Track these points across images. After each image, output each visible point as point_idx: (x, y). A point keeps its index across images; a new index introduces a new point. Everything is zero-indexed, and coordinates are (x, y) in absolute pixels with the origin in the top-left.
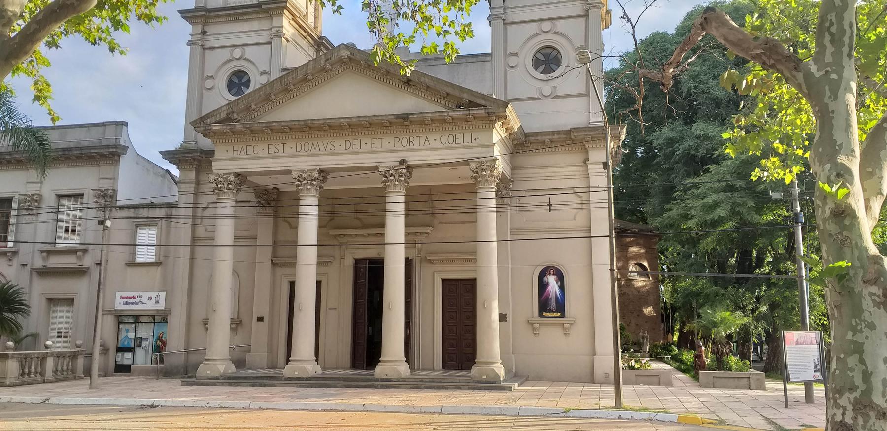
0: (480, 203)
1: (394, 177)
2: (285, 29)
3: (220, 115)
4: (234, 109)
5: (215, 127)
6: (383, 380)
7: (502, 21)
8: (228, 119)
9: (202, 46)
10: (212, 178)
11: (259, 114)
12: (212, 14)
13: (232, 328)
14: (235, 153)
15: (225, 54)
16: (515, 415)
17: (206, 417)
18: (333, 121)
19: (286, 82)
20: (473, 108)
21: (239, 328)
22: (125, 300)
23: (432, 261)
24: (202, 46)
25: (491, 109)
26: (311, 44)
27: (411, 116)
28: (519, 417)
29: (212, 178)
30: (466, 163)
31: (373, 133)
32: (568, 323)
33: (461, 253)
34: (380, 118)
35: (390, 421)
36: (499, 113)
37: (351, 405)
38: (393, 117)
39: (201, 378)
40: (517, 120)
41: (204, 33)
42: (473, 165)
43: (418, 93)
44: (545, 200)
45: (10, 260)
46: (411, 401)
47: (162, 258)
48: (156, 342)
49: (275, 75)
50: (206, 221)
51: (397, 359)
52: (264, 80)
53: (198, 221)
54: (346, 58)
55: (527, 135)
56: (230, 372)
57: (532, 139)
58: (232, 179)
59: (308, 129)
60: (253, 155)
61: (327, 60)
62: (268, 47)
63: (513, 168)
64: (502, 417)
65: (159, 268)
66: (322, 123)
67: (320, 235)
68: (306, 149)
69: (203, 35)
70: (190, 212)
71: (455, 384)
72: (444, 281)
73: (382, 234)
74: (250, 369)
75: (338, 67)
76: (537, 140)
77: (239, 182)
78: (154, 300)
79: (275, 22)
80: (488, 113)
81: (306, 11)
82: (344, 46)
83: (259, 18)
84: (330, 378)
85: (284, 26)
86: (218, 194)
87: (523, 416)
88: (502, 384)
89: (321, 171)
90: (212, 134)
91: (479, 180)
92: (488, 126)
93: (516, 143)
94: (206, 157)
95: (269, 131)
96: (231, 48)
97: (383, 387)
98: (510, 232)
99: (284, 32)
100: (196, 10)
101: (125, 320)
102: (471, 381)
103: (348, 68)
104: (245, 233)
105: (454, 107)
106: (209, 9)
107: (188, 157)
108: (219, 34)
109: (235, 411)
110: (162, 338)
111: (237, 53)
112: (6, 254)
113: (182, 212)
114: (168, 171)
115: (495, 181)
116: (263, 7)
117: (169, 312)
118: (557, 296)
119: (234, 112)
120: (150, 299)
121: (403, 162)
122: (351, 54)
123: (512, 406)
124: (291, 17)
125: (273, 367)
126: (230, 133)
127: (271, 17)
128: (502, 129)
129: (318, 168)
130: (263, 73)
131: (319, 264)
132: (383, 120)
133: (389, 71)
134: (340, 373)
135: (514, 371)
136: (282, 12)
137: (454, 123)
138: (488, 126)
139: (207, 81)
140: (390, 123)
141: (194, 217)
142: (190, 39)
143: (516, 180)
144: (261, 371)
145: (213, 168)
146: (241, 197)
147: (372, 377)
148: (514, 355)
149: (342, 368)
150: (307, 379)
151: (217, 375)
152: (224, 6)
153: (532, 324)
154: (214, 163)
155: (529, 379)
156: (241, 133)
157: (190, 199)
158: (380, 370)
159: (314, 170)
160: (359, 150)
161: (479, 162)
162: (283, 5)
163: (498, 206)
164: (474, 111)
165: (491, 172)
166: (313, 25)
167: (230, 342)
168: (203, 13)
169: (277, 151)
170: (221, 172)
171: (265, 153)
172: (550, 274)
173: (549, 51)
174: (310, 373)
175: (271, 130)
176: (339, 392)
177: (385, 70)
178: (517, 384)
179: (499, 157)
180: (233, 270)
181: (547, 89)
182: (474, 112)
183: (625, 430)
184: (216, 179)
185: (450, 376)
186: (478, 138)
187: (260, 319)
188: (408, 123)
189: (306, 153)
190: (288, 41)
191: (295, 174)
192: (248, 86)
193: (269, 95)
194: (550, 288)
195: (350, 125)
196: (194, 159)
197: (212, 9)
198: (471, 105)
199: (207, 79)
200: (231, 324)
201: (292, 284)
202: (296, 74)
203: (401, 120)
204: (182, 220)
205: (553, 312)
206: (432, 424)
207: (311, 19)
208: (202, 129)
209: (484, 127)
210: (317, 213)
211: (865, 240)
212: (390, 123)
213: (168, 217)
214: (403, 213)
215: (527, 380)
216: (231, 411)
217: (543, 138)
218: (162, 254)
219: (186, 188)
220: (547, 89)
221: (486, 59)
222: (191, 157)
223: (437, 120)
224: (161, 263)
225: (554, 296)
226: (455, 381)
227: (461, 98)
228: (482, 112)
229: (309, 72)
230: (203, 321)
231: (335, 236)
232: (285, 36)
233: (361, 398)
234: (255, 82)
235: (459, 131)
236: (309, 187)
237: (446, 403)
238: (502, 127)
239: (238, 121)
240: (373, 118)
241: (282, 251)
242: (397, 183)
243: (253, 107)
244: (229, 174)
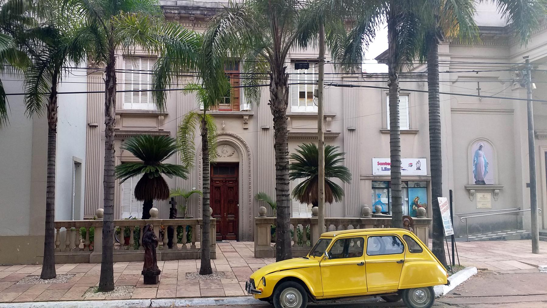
22: (384, 166)
45: (246, 123)
48: (412, 206)
65: (417, 136)
78: (415, 167)
101: (376, 185)
110: (417, 202)
112: (243, 117)
120: (411, 165)
211: (323, 94)
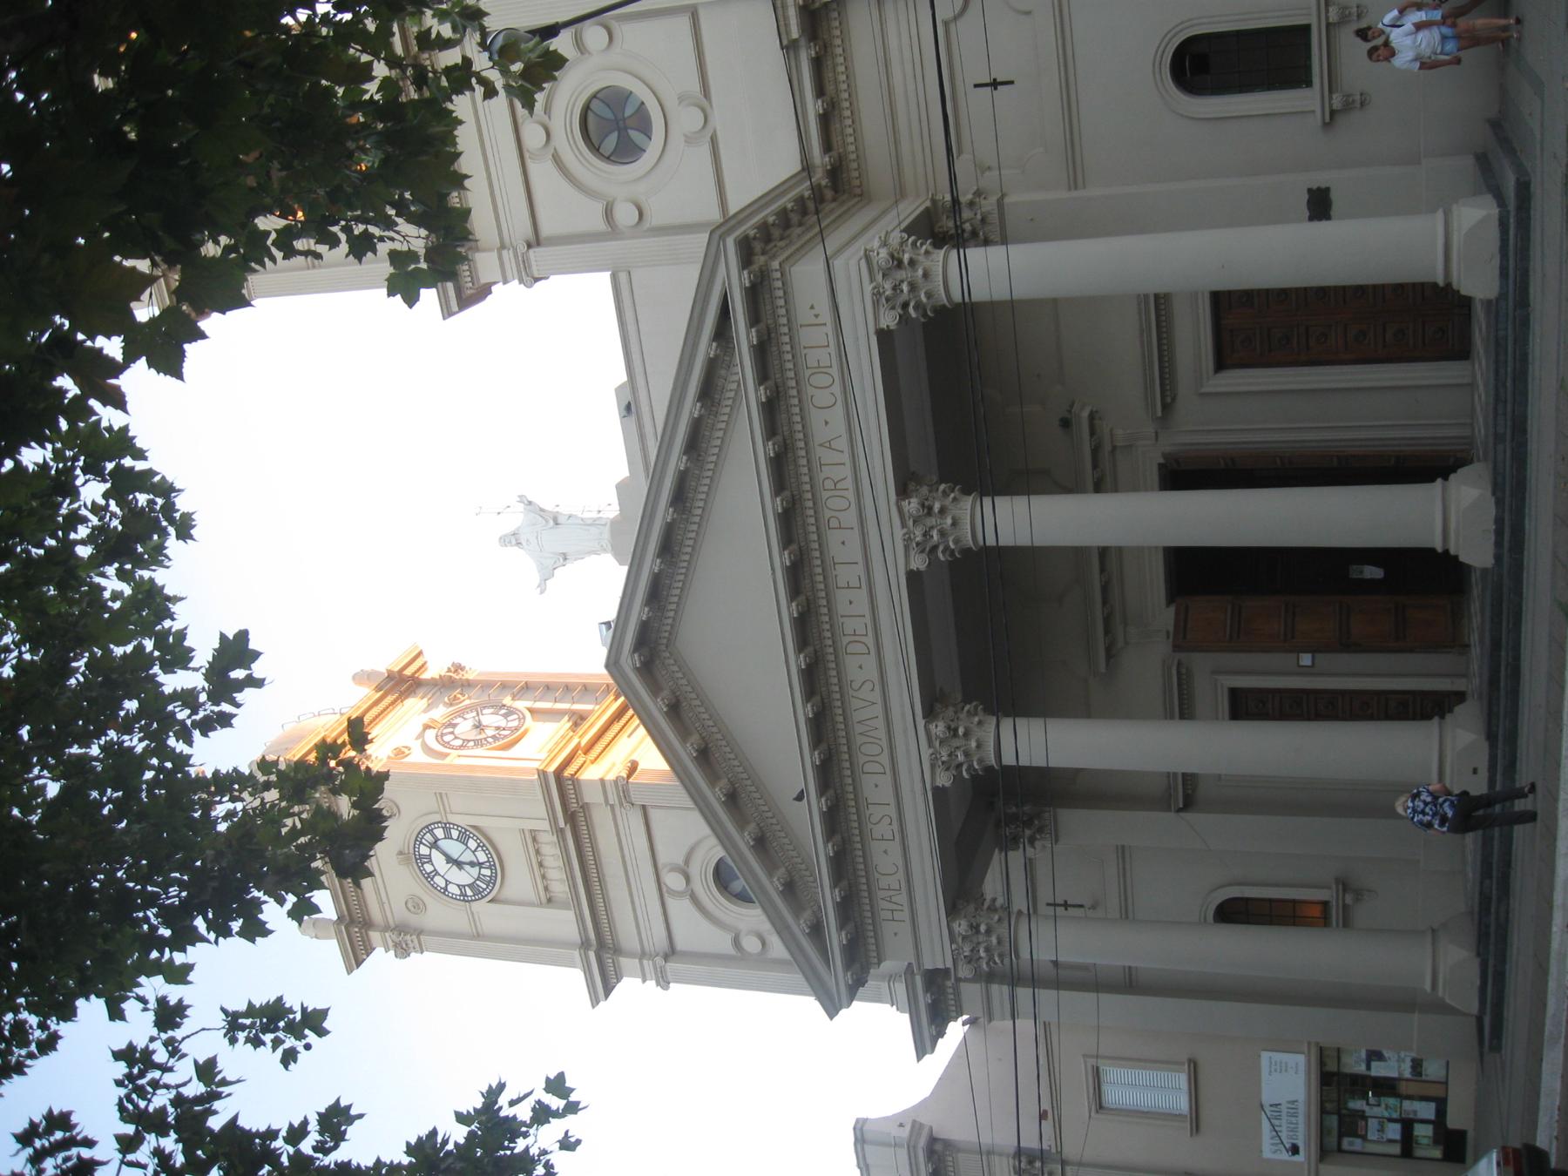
2: (608, 772)
7: (531, 251)
15: (681, 910)
32: (1327, 11)
58: (964, 923)
60: (901, 875)
68: (875, 750)
79: (592, 797)
85: (600, 776)
111: (674, 881)
127: (585, 807)
129: (921, 722)
153: (1333, 113)
158: (1476, 552)
160: (868, 620)
183: (1566, 757)
186: (812, 307)
199: (743, 949)
220: (687, 120)
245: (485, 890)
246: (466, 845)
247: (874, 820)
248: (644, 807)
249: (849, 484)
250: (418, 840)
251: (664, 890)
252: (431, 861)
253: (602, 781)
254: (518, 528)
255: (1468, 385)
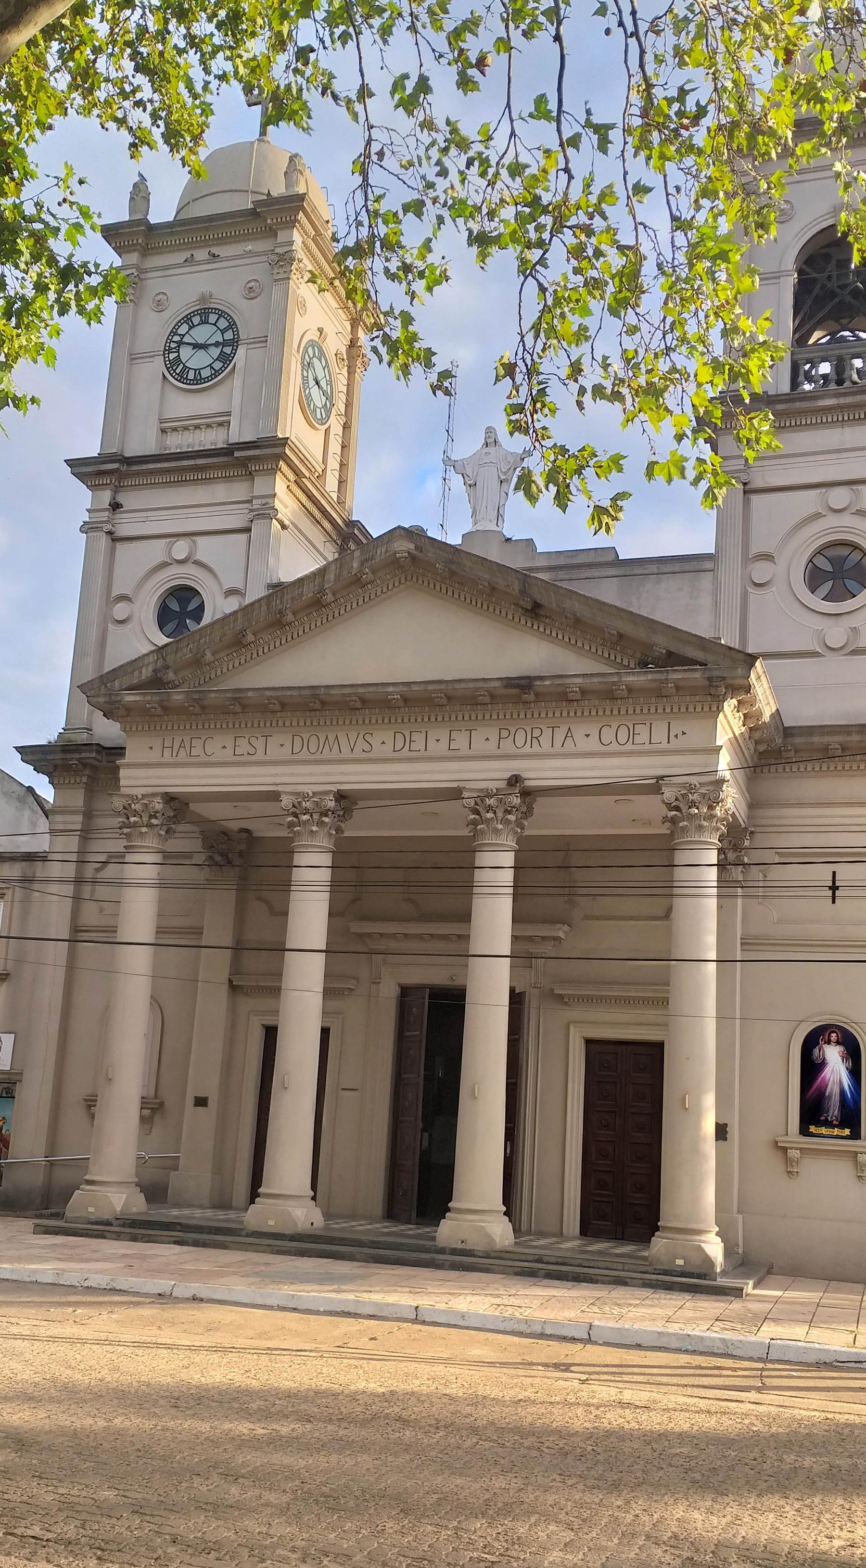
0: (681, 874)
1: (495, 813)
3: (141, 673)
4: (170, 660)
5: (130, 698)
6: (454, 1252)
8: (156, 682)
9: (110, 533)
10: (118, 803)
11: (219, 673)
12: (135, 468)
13: (142, 1119)
14: (167, 752)
15: (156, 551)
16: (760, 1360)
17: (79, 1311)
18: (371, 689)
19: (279, 607)
20: (675, 668)
21: (157, 1119)
23: (566, 1000)
24: (110, 533)
25: (716, 669)
26: (330, 536)
27: (538, 683)
28: (770, 1366)
29: (118, 803)
30: (655, 786)
31: (453, 718)
32: (796, 1149)
33: (629, 984)
34: (471, 685)
35: (476, 1352)
36: (733, 678)
37: (388, 1305)
38: (497, 684)
39: (76, 1220)
40: (770, 698)
41: (115, 506)
42: (669, 794)
43: (554, 634)
44: (822, 873)
46: (520, 1307)
47: (10, 966)
49: (256, 592)
50: (102, 892)
51: (486, 1209)
52: (232, 605)
53: (87, 890)
54: (406, 558)
55: (788, 732)
56: (134, 1210)
57: (798, 740)
59: (318, 706)
60: (203, 758)
61: (367, 560)
62: (243, 537)
63: (753, 805)
64: (728, 1363)
66: (349, 695)
67: (332, 931)
69: (114, 510)
70: (70, 871)
71: (615, 1273)
72: (589, 1042)
73: (459, 936)
74: (177, 1205)
75: (388, 576)
76: (812, 743)
77: (172, 814)
79: (260, 485)
80: (710, 679)
81: (323, 467)
82: (402, 532)
83: (227, 479)
84: (342, 1239)
86: (128, 836)
87: (779, 1361)
88: (721, 1281)
89: (340, 796)
90: (122, 712)
91: (681, 824)
92: (706, 709)
93: (762, 748)
94: (108, 762)
95: (238, 708)
96: (168, 540)
97: (454, 1267)
98: (742, 944)
99: (276, 507)
100: (102, 459)
102: (650, 1269)
103: (409, 578)
104: (176, 922)
105: (632, 665)
106: (128, 458)
107: (72, 759)
108: (146, 510)
109: (141, 1299)
111: (181, 549)
113: (55, 870)
114: (30, 790)
115: (718, 829)
116: (236, 454)
117: (19, 1077)
118: (842, 1092)
119: (168, 668)
121: (514, 780)
122: (417, 548)
123: (752, 1338)
124: (292, 477)
125: (223, 1204)
126: (159, 711)
127: (250, 476)
128: (737, 715)
129: (334, 788)
130: (231, 592)
131: (328, 993)
132: (477, 689)
133: (495, 585)
134: (362, 1228)
135: (740, 1251)
136: (274, 467)
137: (631, 700)
138: (706, 709)
139: (119, 605)
140: (492, 696)
141: (79, 881)
142: (88, 520)
143: (759, 829)
144: (198, 1213)
145: (122, 783)
146: (175, 845)
147: (431, 1243)
148: (740, 1217)
149: (365, 1218)
150: (293, 1238)
151: (107, 1216)
152: (157, 453)
153: (785, 1150)
154: (123, 773)
155: (774, 1270)
156: (181, 711)
157: (73, 843)
159: (327, 793)
160: (423, 753)
161: (683, 785)
162: (277, 450)
163: (722, 883)
164: (677, 675)
165: (711, 808)
166: (335, 496)
167: (140, 1146)
168: (115, 466)
169: (252, 751)
170: (139, 792)
171: (228, 755)
172: (829, 1042)
173: (843, 551)
174: (300, 1225)
175: (244, 706)
176: (357, 1271)
177: (486, 584)
178: (751, 1283)
179: (727, 775)
180: (152, 997)
181: (837, 635)
182: (679, 676)
184: (127, 806)
185: (600, 1253)
186: (684, 733)
187: (201, 1102)
188: (532, 697)
189: (313, 757)
190: (284, 527)
191: (286, 801)
192: (198, 617)
193: (243, 633)
194: (827, 1072)
195: (406, 700)
196: (85, 765)
197: (133, 457)
198: (672, 659)
200: (141, 1109)
201: (271, 1034)
202: (300, 590)
203: (515, 691)
204: (54, 888)
205: (833, 1126)
206: (572, 1368)
207: (331, 484)
208: (102, 700)
209: (699, 709)
210: (329, 884)
212: (492, 696)
213: (27, 881)
214: (511, 890)
215: (769, 1272)
216: (134, 1299)
217: (826, 739)
218: (10, 956)
219: (64, 823)
220: (837, 635)
221: (703, 568)
222: (79, 760)
223: (594, 692)
224: (8, 974)
225: (836, 1091)
226: (615, 1266)
227: (651, 646)
228: (697, 676)
229: (326, 586)
230: (85, 1100)
231: (361, 936)
232: (279, 516)
233: (408, 1289)
234: (214, 609)
235: (641, 717)
236: (315, 828)
237: (600, 1319)
238: (738, 711)
239: (176, 687)
240: (457, 686)
241: (253, 962)
242: (500, 826)
243: (209, 657)
244: (154, 795)
245: (175, 371)
246: (217, 359)
247: (253, 740)
248: (248, 530)
249: (536, 748)
250: (221, 314)
251: (174, 539)
252: (202, 323)
253: (275, 495)
254: (500, 446)
255: (562, 1233)
